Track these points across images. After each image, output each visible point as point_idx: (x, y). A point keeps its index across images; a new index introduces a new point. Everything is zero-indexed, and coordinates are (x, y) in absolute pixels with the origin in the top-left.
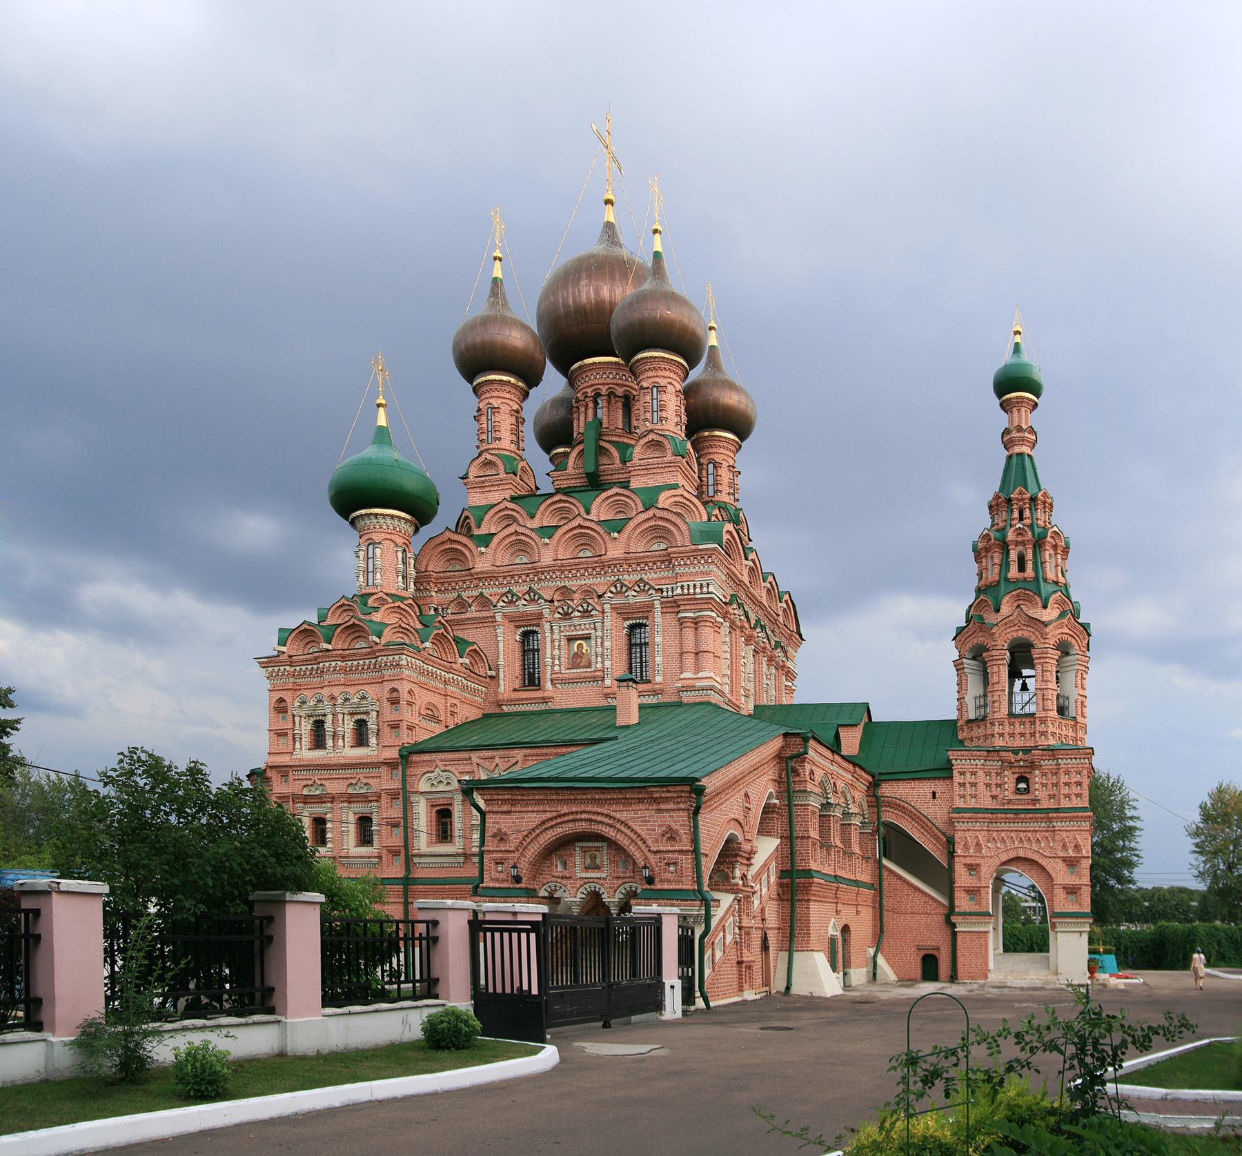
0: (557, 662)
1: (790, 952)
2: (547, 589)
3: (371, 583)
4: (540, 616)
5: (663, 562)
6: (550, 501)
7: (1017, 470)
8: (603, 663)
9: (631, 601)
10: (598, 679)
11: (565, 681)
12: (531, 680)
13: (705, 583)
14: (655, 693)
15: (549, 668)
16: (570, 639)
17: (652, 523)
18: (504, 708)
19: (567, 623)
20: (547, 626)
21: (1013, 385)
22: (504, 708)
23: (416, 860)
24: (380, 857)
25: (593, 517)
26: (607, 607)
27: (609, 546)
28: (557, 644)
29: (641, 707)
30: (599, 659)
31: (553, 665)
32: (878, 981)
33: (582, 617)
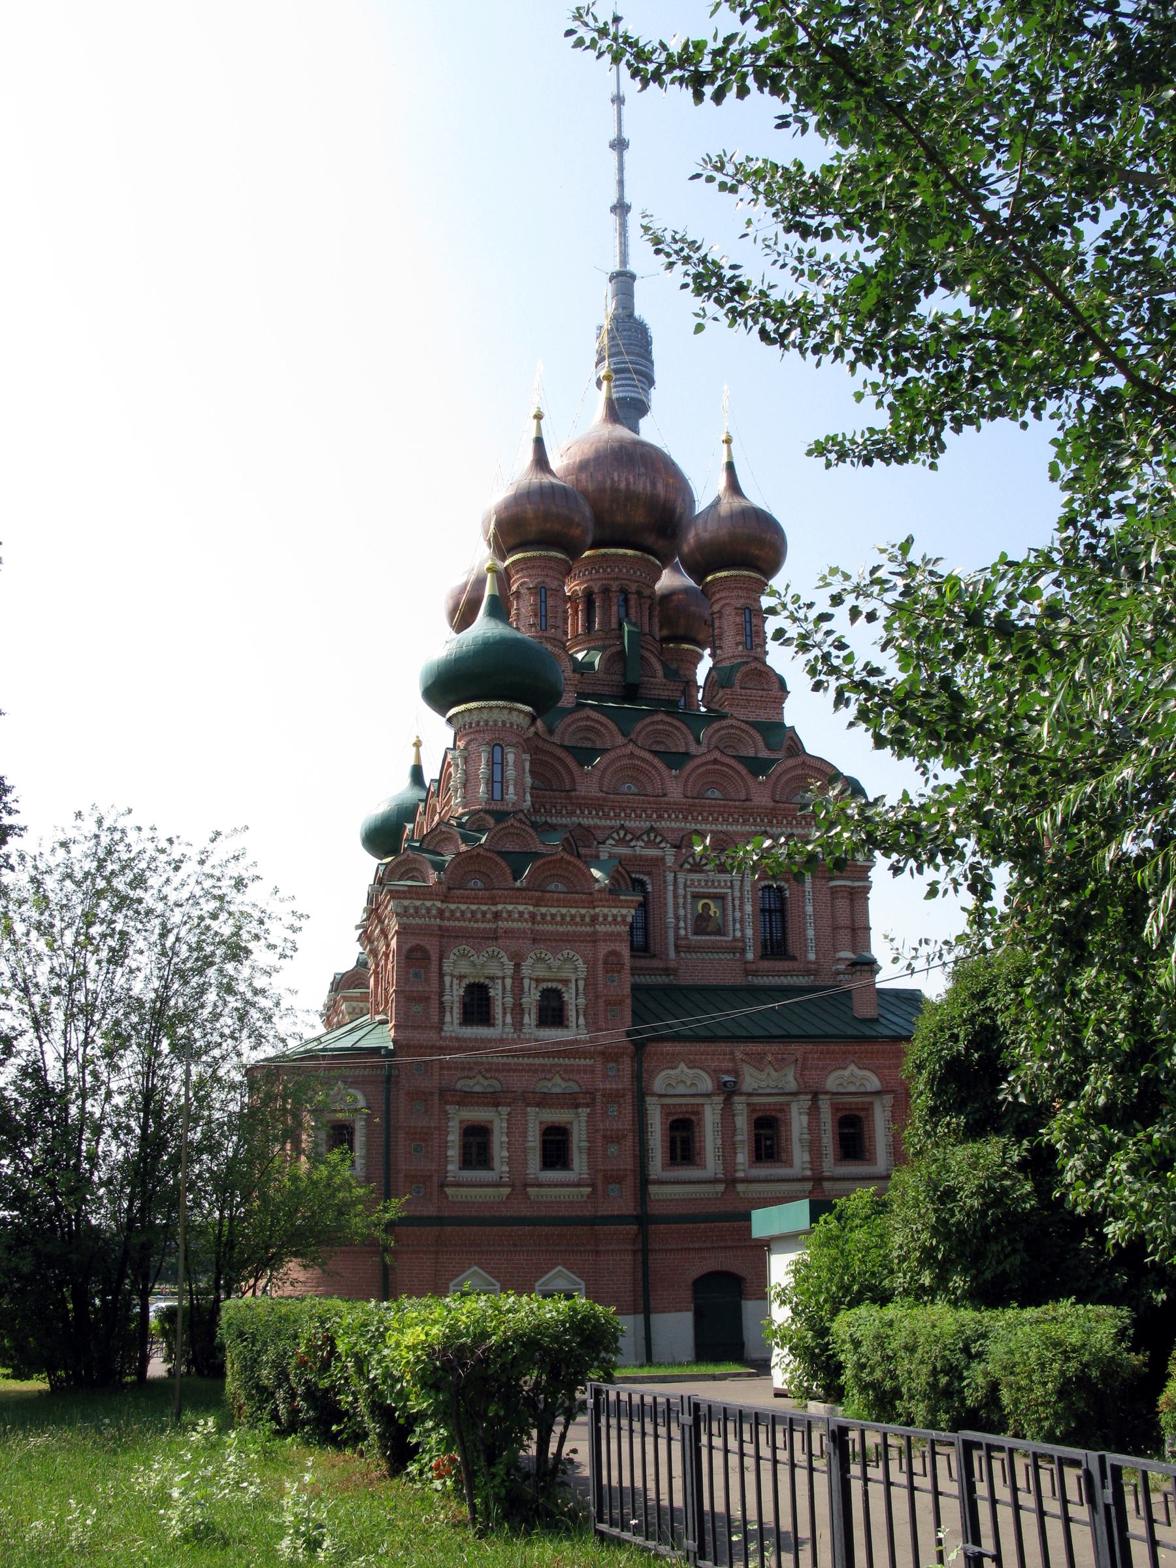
0: (682, 924)
1: (647, 1312)
3: (497, 796)
6: (648, 720)
8: (742, 930)
10: (737, 948)
11: (689, 949)
12: (776, 946)
14: (808, 973)
16: (697, 897)
19: (696, 876)
23: (653, 1189)
25: (556, 739)
27: (578, 780)
28: (681, 901)
29: (635, 988)
30: (738, 926)
31: (677, 928)
32: (655, 1359)
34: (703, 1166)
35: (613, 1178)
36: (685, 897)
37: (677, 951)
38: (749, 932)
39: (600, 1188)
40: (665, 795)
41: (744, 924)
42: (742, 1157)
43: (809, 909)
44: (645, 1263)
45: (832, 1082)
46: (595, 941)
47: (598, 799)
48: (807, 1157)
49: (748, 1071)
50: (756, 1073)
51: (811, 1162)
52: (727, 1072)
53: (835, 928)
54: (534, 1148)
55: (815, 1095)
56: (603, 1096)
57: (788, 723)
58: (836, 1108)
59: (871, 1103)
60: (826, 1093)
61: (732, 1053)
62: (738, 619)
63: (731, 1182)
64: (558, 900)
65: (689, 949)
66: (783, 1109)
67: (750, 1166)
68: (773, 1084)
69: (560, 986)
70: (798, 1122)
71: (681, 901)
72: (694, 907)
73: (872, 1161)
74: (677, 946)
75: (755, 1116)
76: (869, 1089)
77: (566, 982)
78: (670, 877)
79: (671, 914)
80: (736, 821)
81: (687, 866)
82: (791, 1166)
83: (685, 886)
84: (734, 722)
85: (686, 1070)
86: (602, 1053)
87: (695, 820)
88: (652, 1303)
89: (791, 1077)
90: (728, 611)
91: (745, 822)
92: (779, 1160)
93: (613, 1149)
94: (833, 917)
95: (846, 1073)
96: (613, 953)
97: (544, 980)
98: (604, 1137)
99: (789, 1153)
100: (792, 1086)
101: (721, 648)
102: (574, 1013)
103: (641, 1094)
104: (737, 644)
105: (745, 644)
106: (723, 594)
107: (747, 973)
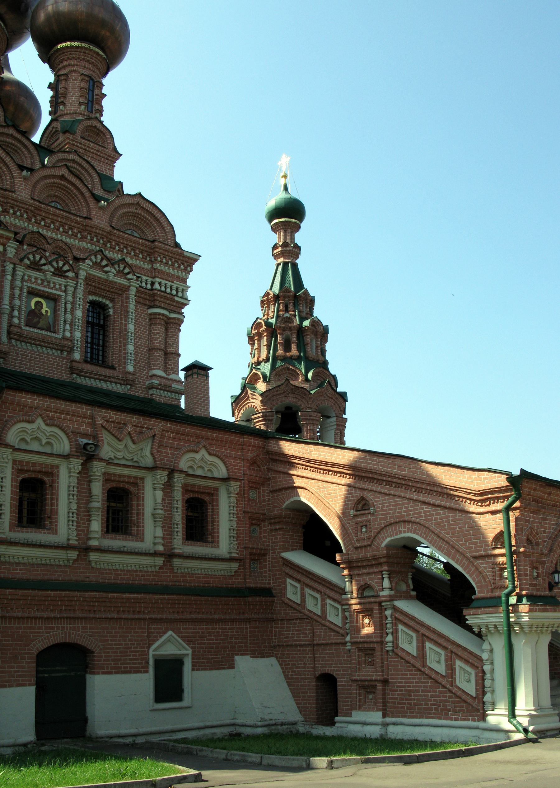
10: (65, 347)
11: (21, 338)
13: (180, 289)
14: (126, 382)
15: (5, 319)
16: (32, 293)
19: (34, 274)
20: (9, 267)
28: (17, 292)
30: (68, 327)
31: (11, 316)
33: (54, 274)
34: (55, 532)
36: (21, 289)
37: (9, 338)
38: (78, 335)
40: (14, 192)
41: (73, 327)
42: (96, 526)
48: (159, 532)
49: (106, 438)
50: (114, 442)
52: (85, 436)
53: (151, 350)
54: (88, 168)
55: (172, 472)
57: (117, 178)
58: (186, 489)
59: (217, 489)
60: (181, 471)
61: (92, 417)
62: (83, 85)
63: (85, 550)
65: (21, 338)
66: (137, 483)
67: (103, 536)
70: (151, 498)
71: (17, 292)
72: (28, 303)
73: (214, 542)
74: (9, 333)
75: (109, 486)
76: (216, 475)
78: (9, 267)
79: (6, 301)
80: (75, 235)
81: (27, 262)
82: (142, 540)
83: (23, 280)
85: (43, 426)
87: (38, 223)
89: (147, 452)
90: (74, 76)
91: (83, 238)
92: (126, 534)
94: (150, 340)
95: (198, 456)
99: (140, 526)
100: (148, 461)
101: (63, 103)
104: (80, 104)
105: (87, 105)
106: (72, 62)
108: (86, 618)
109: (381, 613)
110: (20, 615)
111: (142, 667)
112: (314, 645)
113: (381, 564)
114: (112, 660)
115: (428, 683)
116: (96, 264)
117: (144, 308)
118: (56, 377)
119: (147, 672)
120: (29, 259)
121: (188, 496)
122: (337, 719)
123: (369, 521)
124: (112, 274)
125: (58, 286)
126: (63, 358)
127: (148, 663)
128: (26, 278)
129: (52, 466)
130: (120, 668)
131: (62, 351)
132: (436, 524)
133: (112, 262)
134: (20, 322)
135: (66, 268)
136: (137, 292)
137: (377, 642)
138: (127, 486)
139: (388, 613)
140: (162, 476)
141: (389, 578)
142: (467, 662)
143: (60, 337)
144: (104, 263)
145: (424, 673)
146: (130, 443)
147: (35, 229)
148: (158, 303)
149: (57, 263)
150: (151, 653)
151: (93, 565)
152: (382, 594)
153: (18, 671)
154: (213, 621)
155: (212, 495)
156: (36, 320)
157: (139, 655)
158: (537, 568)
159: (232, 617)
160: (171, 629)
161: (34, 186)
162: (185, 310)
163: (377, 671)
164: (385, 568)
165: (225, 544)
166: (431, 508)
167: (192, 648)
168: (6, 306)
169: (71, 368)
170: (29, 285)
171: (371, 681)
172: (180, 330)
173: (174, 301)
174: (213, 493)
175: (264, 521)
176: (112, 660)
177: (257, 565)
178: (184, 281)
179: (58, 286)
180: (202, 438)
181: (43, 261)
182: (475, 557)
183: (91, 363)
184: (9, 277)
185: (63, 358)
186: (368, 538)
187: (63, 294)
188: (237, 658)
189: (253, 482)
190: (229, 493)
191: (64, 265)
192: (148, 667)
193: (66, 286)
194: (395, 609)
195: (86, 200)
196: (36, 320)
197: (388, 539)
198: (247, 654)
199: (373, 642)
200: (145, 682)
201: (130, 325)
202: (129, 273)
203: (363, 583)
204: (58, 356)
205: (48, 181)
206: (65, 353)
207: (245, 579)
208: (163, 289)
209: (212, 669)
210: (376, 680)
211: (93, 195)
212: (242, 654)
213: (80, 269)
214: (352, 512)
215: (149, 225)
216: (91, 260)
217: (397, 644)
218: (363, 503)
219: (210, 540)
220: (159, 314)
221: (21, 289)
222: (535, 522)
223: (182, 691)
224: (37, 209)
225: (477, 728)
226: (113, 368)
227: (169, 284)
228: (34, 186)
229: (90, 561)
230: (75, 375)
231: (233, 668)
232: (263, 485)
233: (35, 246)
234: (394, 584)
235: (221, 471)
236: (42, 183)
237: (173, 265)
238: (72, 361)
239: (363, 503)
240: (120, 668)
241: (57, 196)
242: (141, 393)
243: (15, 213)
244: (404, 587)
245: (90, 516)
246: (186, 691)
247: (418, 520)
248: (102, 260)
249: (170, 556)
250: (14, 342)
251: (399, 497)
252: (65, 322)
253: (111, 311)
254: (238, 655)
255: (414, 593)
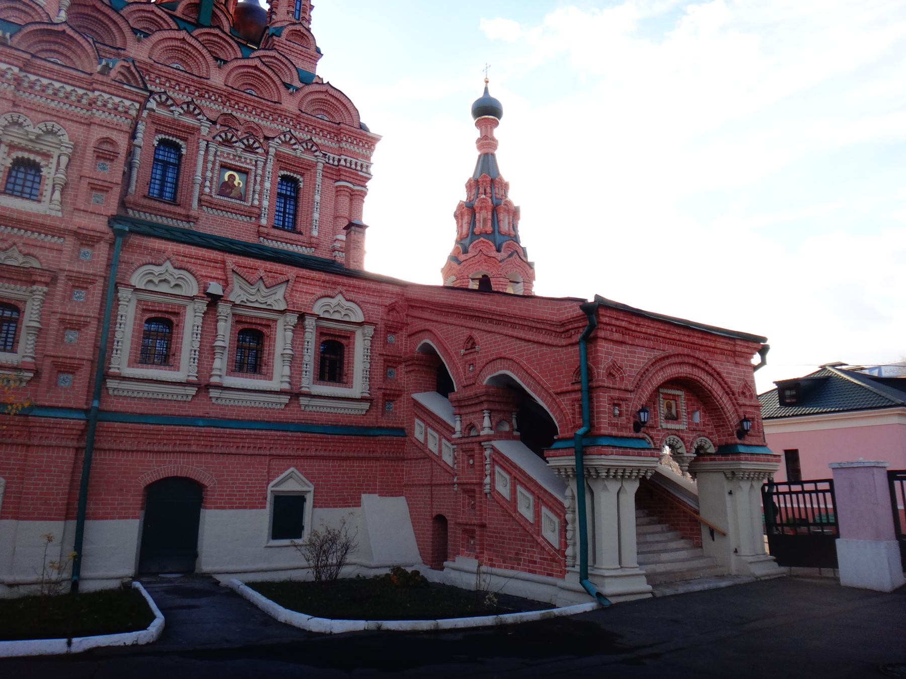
2: (213, 108)
4: (193, 131)
5: (329, 133)
7: (487, 162)
8: (260, 201)
9: (298, 155)
10: (254, 214)
11: (211, 205)
14: (310, 245)
15: (197, 189)
17: (322, 96)
18: (130, 212)
19: (227, 150)
20: (203, 144)
21: (487, 111)
22: (130, 212)
23: (111, 384)
24: (37, 373)
26: (272, 151)
28: (210, 166)
30: (257, 196)
31: (202, 186)
33: (245, 150)
35: (65, 367)
36: (214, 163)
38: (266, 203)
39: (45, 375)
42: (220, 363)
43: (317, 198)
44: (88, 461)
45: (318, 309)
46: (89, 125)
47: (145, 63)
49: (236, 282)
50: (246, 286)
51: (290, 377)
53: (336, 217)
55: (302, 317)
56: (69, 278)
59: (353, 333)
61: (224, 262)
64: (51, 71)
68: (264, 300)
69: (38, 159)
70: (281, 339)
71: (210, 166)
72: (220, 176)
73: (348, 384)
74: (200, 200)
76: (353, 320)
77: (47, 156)
79: (199, 172)
84: (277, 55)
85: (171, 269)
86: (76, 234)
88: (91, 507)
92: (260, 373)
93: (71, 336)
95: (333, 302)
96: (107, 140)
97: (23, 149)
98: (62, 321)
101: (276, 14)
102: (49, 188)
103: (113, 284)
107: (259, 235)
108: (201, 453)
109: (482, 454)
110: (128, 448)
111: (260, 503)
112: (431, 485)
113: (482, 402)
114: (227, 495)
115: (517, 530)
116: (285, 142)
117: (331, 181)
118: (244, 240)
119: (264, 508)
120: (221, 136)
121: (324, 339)
122: (445, 563)
123: (475, 359)
124: (300, 151)
125: (248, 161)
126: (252, 223)
127: (266, 499)
128: (219, 153)
129: (179, 306)
130: (235, 503)
131: (251, 217)
132: (527, 360)
133: (299, 142)
134: (211, 192)
135: (256, 145)
136: (324, 167)
137: (476, 484)
138: (259, 328)
139: (487, 453)
140: (293, 319)
141: (490, 417)
142: (551, 509)
143: (249, 204)
144: (293, 141)
145: (514, 519)
146: (263, 287)
147: (230, 112)
148: (343, 177)
149: (248, 140)
150: (270, 488)
151: (111, 392)
152: (482, 433)
153: (122, 504)
154: (340, 458)
155: (348, 338)
156: (228, 191)
157: (257, 491)
158: (619, 405)
159: (361, 455)
160: (294, 466)
161: (229, 74)
162: (369, 184)
163: (475, 515)
164: (485, 406)
165: (358, 386)
166: (523, 343)
167: (315, 485)
168: (199, 178)
169: (258, 231)
170: (222, 159)
171: (471, 525)
172: (363, 201)
173: (358, 175)
174: (349, 336)
175: (400, 363)
176: (227, 495)
177: (392, 405)
178: (368, 158)
179: (248, 161)
180: (339, 284)
181: (234, 139)
182: (557, 394)
183: (283, 229)
184: (202, 153)
185: (252, 223)
186: (473, 377)
187: (253, 168)
188: (363, 496)
189: (390, 327)
190: (364, 335)
191: (254, 142)
192: (265, 503)
193: (256, 161)
194: (493, 448)
195: (278, 88)
196: (228, 191)
197: (489, 377)
198: (375, 493)
199: (472, 484)
200: (262, 519)
201: (318, 196)
202: (316, 151)
203: (468, 422)
204: (247, 222)
205: (245, 70)
206: (253, 219)
207: (377, 419)
208: (348, 165)
209: (336, 507)
210: (474, 525)
211: (284, 84)
212: (370, 493)
213: (269, 147)
214: (463, 351)
215: (337, 110)
216: (280, 138)
217: (494, 487)
218: (471, 342)
219: (345, 380)
220: (344, 186)
221: (214, 163)
222: (618, 355)
223: (302, 528)
224: (230, 94)
225: (554, 585)
226: (300, 233)
227: (354, 161)
228: (229, 74)
229: (107, 389)
230: (262, 239)
231: (360, 506)
232: (401, 329)
233: (227, 126)
234: (494, 424)
235: (358, 316)
236: (236, 72)
237: (357, 144)
238: (259, 226)
239: (471, 342)
240: (235, 503)
241: (250, 84)
242: (326, 256)
243: (210, 98)
244: (506, 428)
245: (214, 354)
246: (305, 528)
247: (511, 356)
248: (291, 139)
249: (295, 395)
250: (204, 208)
251: (499, 333)
252: (254, 191)
253: (301, 185)
254: (365, 493)
255: (516, 433)
